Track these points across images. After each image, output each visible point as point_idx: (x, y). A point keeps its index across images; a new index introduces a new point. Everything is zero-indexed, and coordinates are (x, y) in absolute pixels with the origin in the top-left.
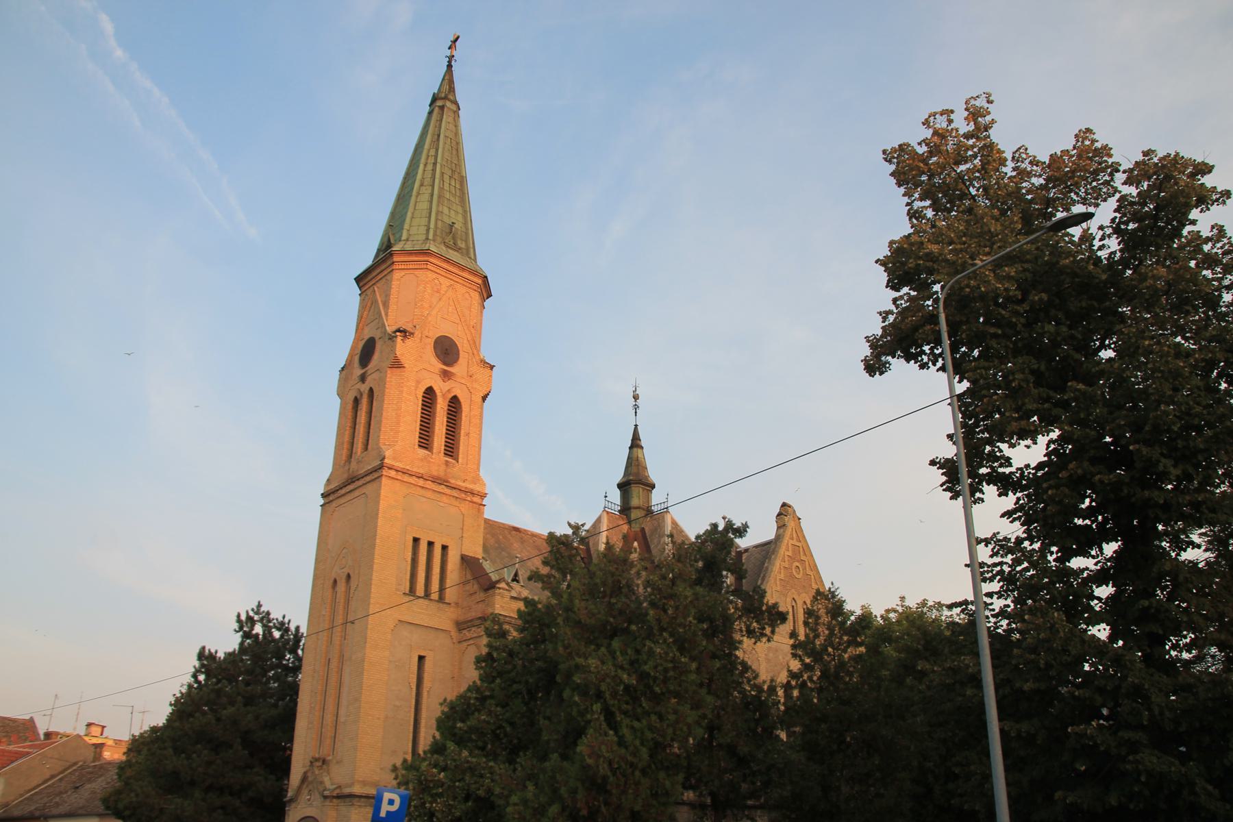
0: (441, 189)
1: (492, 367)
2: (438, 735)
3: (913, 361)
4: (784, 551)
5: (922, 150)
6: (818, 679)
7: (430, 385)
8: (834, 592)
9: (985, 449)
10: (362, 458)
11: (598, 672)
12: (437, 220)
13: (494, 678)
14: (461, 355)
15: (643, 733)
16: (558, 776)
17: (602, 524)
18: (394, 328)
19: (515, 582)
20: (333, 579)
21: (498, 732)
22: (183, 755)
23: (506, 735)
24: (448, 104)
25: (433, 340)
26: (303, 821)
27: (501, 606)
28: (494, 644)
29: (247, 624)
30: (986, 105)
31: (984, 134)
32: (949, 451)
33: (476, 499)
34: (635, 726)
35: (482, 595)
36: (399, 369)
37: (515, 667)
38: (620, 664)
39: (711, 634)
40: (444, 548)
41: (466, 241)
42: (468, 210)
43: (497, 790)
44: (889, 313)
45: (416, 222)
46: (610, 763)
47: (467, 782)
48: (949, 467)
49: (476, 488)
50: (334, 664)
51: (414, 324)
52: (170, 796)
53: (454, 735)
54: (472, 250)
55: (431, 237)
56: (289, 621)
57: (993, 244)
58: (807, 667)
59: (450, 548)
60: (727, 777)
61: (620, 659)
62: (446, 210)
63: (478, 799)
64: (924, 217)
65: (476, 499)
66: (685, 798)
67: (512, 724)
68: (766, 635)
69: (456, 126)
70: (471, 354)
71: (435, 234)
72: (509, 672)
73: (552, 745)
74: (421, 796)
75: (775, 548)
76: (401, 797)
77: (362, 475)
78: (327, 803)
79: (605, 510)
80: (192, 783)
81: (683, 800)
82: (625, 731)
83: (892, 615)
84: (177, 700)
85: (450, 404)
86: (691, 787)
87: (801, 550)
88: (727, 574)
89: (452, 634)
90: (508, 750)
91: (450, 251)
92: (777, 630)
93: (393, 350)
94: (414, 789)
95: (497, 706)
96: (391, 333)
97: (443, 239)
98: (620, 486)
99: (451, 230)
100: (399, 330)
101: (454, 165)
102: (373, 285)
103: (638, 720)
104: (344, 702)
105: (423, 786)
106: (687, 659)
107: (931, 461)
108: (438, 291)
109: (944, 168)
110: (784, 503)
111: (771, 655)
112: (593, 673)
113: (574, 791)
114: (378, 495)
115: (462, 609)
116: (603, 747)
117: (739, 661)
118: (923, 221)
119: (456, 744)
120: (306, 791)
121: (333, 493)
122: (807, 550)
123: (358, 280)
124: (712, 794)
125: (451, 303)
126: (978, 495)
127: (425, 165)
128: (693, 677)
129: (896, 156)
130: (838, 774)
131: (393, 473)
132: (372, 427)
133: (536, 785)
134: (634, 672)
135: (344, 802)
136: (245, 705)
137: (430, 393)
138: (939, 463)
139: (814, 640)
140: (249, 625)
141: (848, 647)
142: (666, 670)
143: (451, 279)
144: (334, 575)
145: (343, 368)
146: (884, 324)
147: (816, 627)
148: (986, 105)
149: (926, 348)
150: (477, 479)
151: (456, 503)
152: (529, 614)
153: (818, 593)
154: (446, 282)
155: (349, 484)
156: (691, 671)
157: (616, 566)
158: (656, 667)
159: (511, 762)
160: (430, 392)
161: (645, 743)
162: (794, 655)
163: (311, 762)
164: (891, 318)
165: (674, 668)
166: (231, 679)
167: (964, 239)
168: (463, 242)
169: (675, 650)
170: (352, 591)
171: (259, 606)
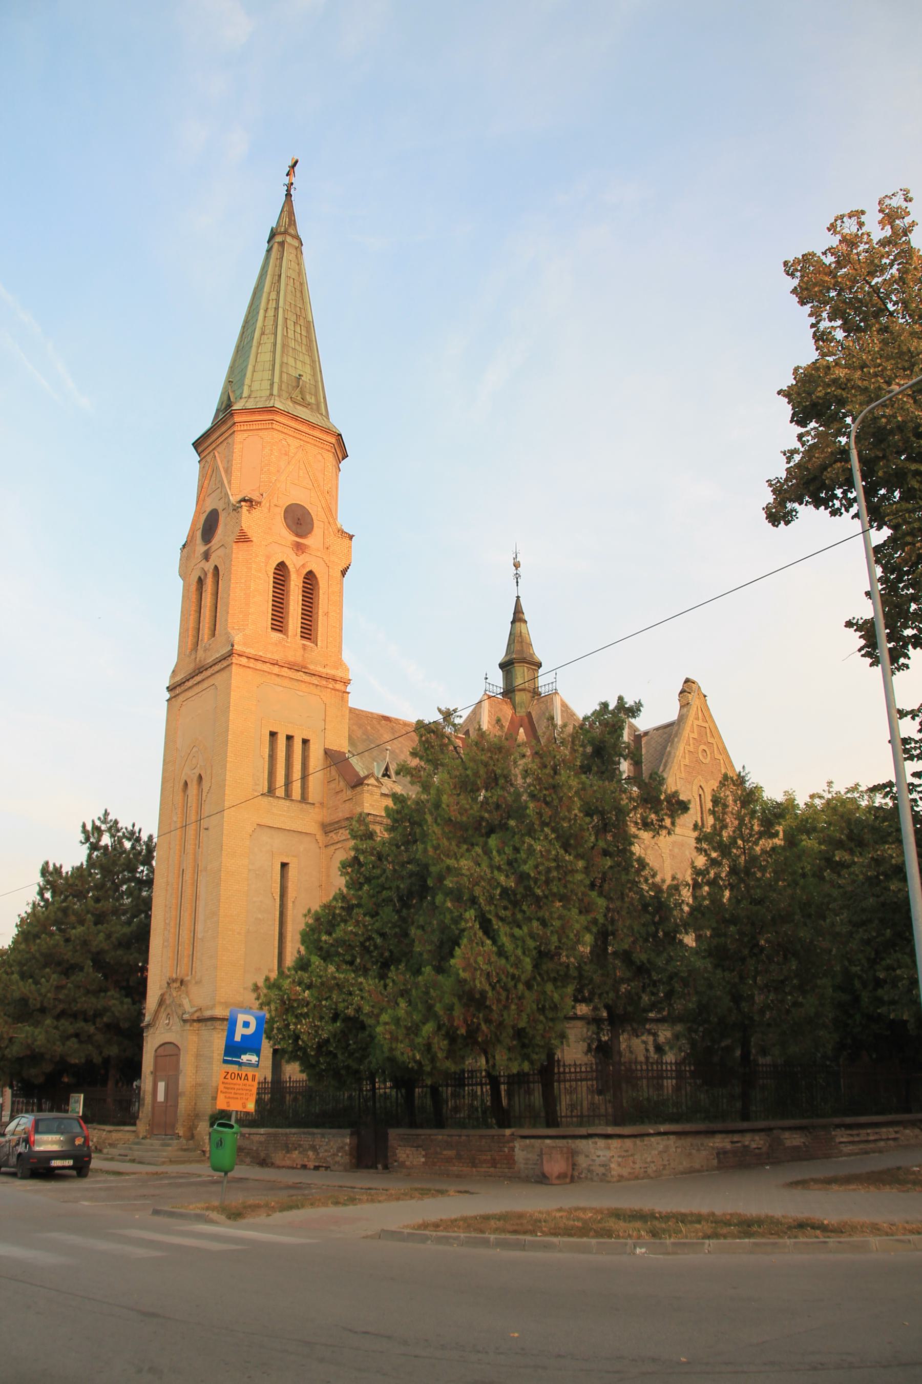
0: (285, 337)
1: (351, 537)
2: (302, 949)
3: (823, 507)
4: (688, 733)
5: (829, 260)
6: (726, 876)
7: (281, 560)
8: (743, 777)
9: (910, 606)
11: (471, 874)
12: (281, 372)
13: (361, 885)
14: (315, 525)
15: (524, 941)
16: (432, 991)
17: (482, 710)
18: (239, 498)
19: (386, 778)
20: (183, 781)
21: (367, 944)
22: (30, 980)
23: (376, 947)
24: (289, 239)
25: (283, 510)
26: (163, 1047)
27: (370, 805)
28: (361, 847)
29: (93, 835)
30: (904, 204)
31: (904, 239)
32: (866, 610)
33: (339, 686)
34: (516, 934)
35: (349, 793)
36: (245, 544)
37: (384, 871)
38: (497, 864)
39: (604, 828)
40: (305, 742)
41: (316, 395)
42: (317, 359)
43: (367, 1009)
44: (794, 452)
45: (258, 376)
46: (488, 975)
47: (334, 1000)
48: (867, 629)
49: (339, 674)
50: (188, 876)
52: (19, 1025)
53: (321, 949)
54: (323, 405)
55: (275, 392)
56: (140, 830)
57: (913, 365)
58: (714, 862)
60: (623, 988)
61: (497, 859)
62: (291, 362)
63: (347, 1019)
64: (833, 339)
66: (579, 1013)
67: (383, 935)
68: (666, 828)
69: (298, 264)
70: (327, 523)
71: (280, 389)
72: (378, 878)
73: (425, 956)
74: (284, 1017)
75: (679, 728)
76: (257, 1019)
77: (211, 664)
78: (188, 1026)
79: (485, 694)
80: (43, 1010)
81: (575, 1014)
82: (504, 939)
83: (818, 802)
84: (22, 920)
85: (276, 571)
86: (584, 1000)
87: (708, 731)
88: (619, 759)
89: (318, 837)
90: (379, 964)
91: (298, 407)
92: (677, 821)
93: (238, 522)
94: (276, 1009)
95: (365, 915)
96: (235, 503)
98: (502, 666)
99: (299, 383)
100: (244, 500)
101: (298, 309)
102: (214, 449)
103: (520, 927)
104: (201, 916)
105: (287, 1006)
106: (571, 857)
107: (846, 622)
109: (855, 281)
110: (687, 678)
111: (676, 850)
112: (466, 876)
113: (450, 1008)
114: (228, 687)
115: (328, 809)
116: (480, 959)
117: (635, 857)
118: (832, 344)
119: (321, 959)
120: (164, 1016)
121: (179, 685)
122: (714, 732)
123: (196, 445)
124: (607, 1007)
125: (302, 466)
126: (902, 660)
127: (266, 311)
128: (579, 877)
129: (799, 268)
130: (751, 982)
131: (244, 661)
132: (218, 610)
133: (410, 1002)
134: (513, 873)
135: (206, 1026)
136: (96, 924)
138: (856, 624)
139: (721, 831)
140: (96, 835)
141: (760, 838)
142: (549, 870)
144: (184, 778)
145: (184, 546)
146: (789, 466)
147: (723, 816)
148: (904, 204)
149: (839, 492)
150: (339, 664)
151: (316, 691)
152: (398, 812)
153: (726, 777)
154: (294, 443)
155: (197, 675)
156: (577, 871)
157: (489, 755)
158: (536, 867)
159: (382, 977)
161: (527, 953)
162: (699, 850)
163: (168, 984)
164: (797, 458)
165: (558, 867)
166: (80, 895)
167: (878, 361)
168: (313, 397)
169: (557, 847)
170: (204, 794)
171: (106, 814)
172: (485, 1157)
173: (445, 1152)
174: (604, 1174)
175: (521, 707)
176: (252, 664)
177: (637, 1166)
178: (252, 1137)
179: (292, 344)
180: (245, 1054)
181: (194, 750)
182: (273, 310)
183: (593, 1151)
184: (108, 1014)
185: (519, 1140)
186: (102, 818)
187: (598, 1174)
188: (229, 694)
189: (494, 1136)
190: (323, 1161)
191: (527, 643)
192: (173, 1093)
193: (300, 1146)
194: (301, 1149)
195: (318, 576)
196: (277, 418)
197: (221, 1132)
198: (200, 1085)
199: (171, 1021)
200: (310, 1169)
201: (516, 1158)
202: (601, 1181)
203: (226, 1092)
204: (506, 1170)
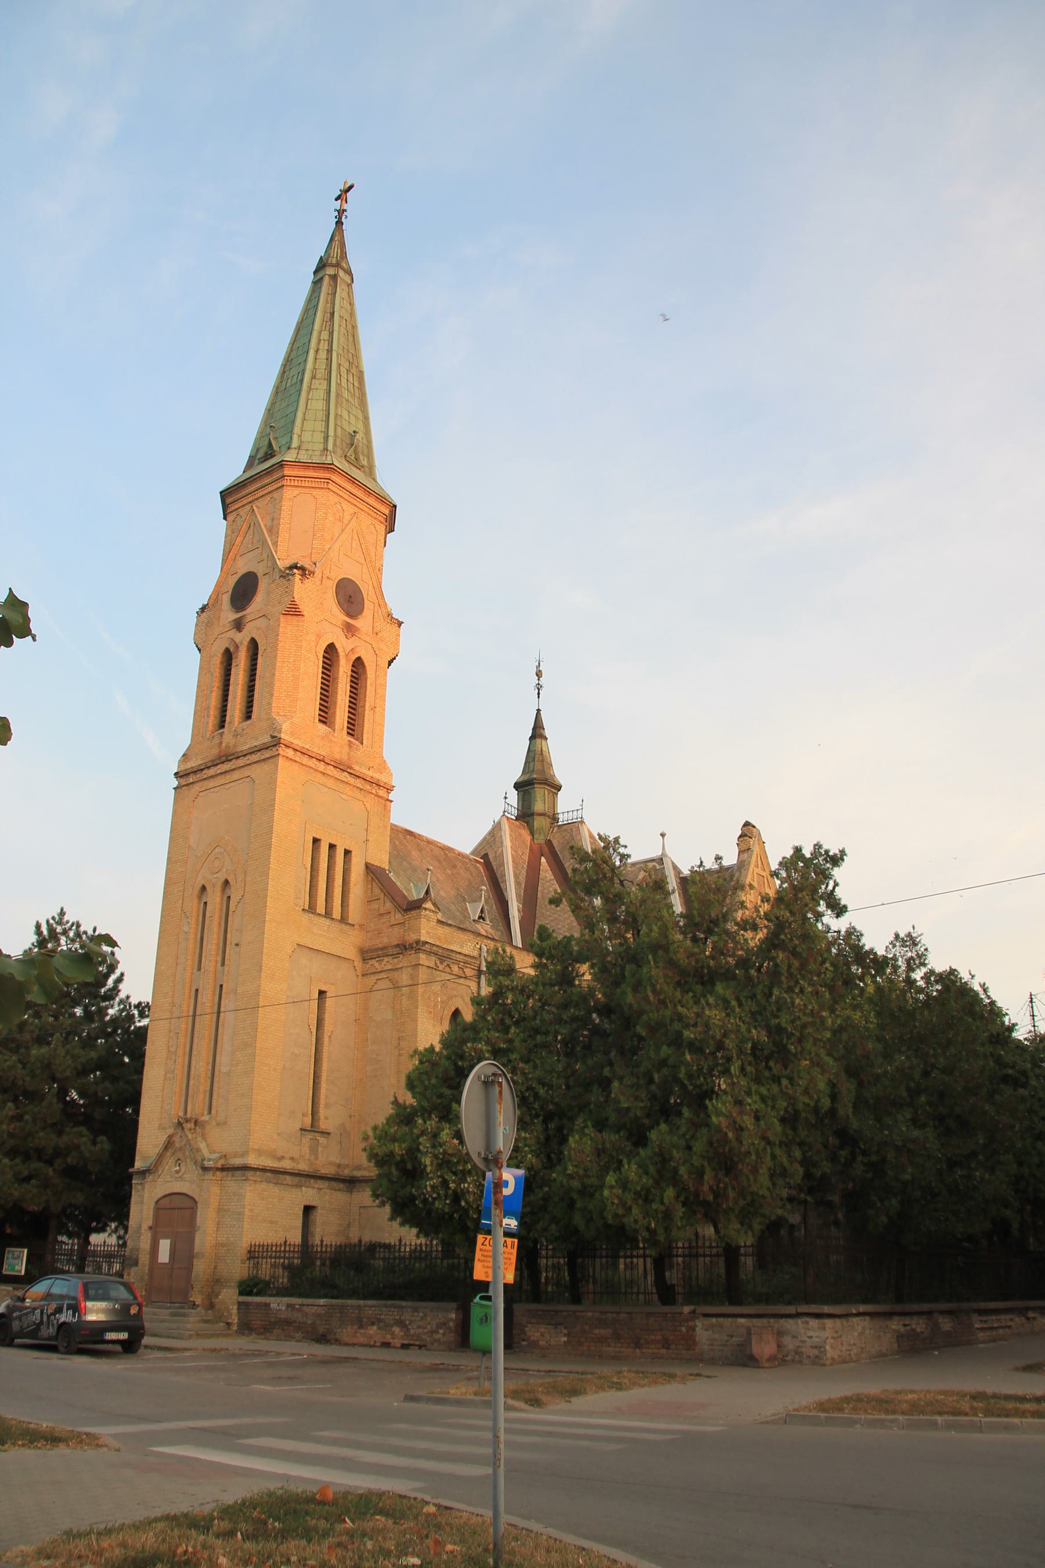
0: (339, 385)
1: (400, 624)
10: (243, 730)
12: (336, 425)
18: (288, 563)
24: (341, 273)
25: (335, 584)
33: (382, 792)
35: (399, 917)
40: (347, 853)
45: (309, 425)
49: (382, 778)
51: (313, 560)
55: (330, 447)
62: (345, 415)
70: (377, 605)
71: (335, 445)
78: (209, 1176)
79: (504, 815)
85: (326, 655)
93: (289, 591)
97: (344, 451)
98: (517, 786)
100: (295, 566)
105: (440, 1161)
108: (340, 520)
113: (701, 1174)
115: (368, 932)
120: (172, 1161)
121: (195, 772)
125: (355, 536)
127: (317, 351)
131: (290, 753)
135: (233, 1176)
137: (331, 651)
143: (355, 505)
145: (203, 609)
150: (383, 767)
151: (358, 795)
154: (349, 509)
155: (223, 763)
158: (793, 1022)
160: (331, 649)
168: (366, 459)
171: (62, 913)
172: (653, 1337)
173: (597, 1331)
174: (817, 1357)
175: (540, 833)
176: (298, 757)
177: (844, 1348)
178: (305, 1308)
179: (345, 394)
181: (216, 850)
182: (325, 352)
183: (803, 1331)
184: (74, 1153)
185: (701, 1318)
186: (57, 918)
187: (809, 1357)
188: (274, 790)
189: (666, 1314)
190: (415, 1338)
191: (547, 763)
192: (184, 1254)
193: (380, 1320)
194: (382, 1324)
195: (366, 664)
196: (334, 478)
198: (223, 1245)
199: (183, 1169)
201: (697, 1339)
202: (814, 1363)
203: (484, 1261)
204: (684, 1352)
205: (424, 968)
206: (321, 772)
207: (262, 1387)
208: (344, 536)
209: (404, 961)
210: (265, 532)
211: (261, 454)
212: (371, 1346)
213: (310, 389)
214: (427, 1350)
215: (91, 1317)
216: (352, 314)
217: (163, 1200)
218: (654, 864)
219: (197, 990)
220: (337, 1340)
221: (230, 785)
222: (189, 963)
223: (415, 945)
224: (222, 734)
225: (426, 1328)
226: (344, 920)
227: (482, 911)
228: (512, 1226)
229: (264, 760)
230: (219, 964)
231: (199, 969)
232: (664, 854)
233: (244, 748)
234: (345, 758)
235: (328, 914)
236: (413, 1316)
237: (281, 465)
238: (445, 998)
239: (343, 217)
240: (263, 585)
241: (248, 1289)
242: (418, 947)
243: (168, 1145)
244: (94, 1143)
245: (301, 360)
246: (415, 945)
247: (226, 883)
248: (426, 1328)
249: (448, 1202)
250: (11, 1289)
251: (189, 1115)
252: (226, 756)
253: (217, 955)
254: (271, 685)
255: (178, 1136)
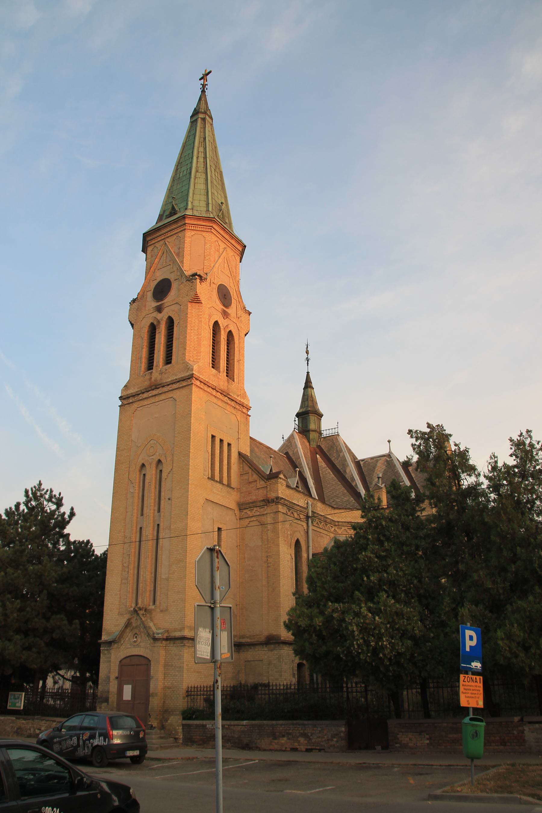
0: (211, 177)
1: (250, 313)
10: (166, 370)
12: (212, 198)
24: (207, 117)
25: (217, 287)
33: (245, 410)
35: (262, 483)
40: (229, 445)
45: (197, 197)
49: (245, 402)
55: (210, 209)
59: (232, 445)
62: (216, 194)
65: (245, 411)
70: (238, 302)
71: (212, 209)
78: (158, 644)
79: (294, 430)
97: (217, 213)
98: (298, 415)
100: (195, 275)
108: (218, 251)
115: (241, 493)
121: (133, 396)
125: (226, 261)
127: (198, 157)
131: (198, 383)
135: (174, 643)
143: (225, 243)
144: (140, 461)
145: (134, 301)
150: (244, 396)
151: (234, 412)
154: (222, 246)
155: (153, 390)
160: (216, 324)
171: (40, 484)
172: (493, 738)
173: (451, 736)
175: (313, 442)
176: (202, 386)
178: (232, 727)
179: (215, 183)
180: (473, 662)
181: (151, 442)
182: (203, 158)
188: (190, 405)
193: (289, 734)
194: (290, 736)
196: (215, 226)
197: (477, 725)
198: (169, 688)
199: (139, 640)
200: (301, 751)
201: (526, 738)
205: (281, 513)
206: (214, 396)
207: (299, 792)
208: (220, 260)
209: (268, 510)
210: (175, 256)
211: (167, 213)
212: (284, 751)
213: (196, 177)
214: (325, 752)
215: (117, 741)
216: (214, 140)
217: (124, 661)
218: (385, 458)
219: (141, 528)
220: (257, 747)
221: (158, 403)
222: (135, 511)
223: (275, 500)
224: (151, 373)
225: (324, 738)
226: (229, 485)
227: (297, 483)
228: (479, 668)
229: (182, 387)
230: (156, 512)
231: (142, 515)
232: (390, 452)
233: (167, 381)
234: (226, 388)
235: (221, 482)
236: (313, 730)
237: (184, 217)
238: (291, 532)
239: (205, 89)
240: (175, 286)
241: (189, 716)
242: (277, 501)
243: (128, 625)
244: (70, 623)
245: (188, 162)
246: (275, 500)
247: (159, 461)
248: (324, 738)
249: (369, 655)
250: (14, 718)
251: (140, 605)
252: (156, 386)
253: (155, 506)
254: (184, 344)
255: (135, 618)
